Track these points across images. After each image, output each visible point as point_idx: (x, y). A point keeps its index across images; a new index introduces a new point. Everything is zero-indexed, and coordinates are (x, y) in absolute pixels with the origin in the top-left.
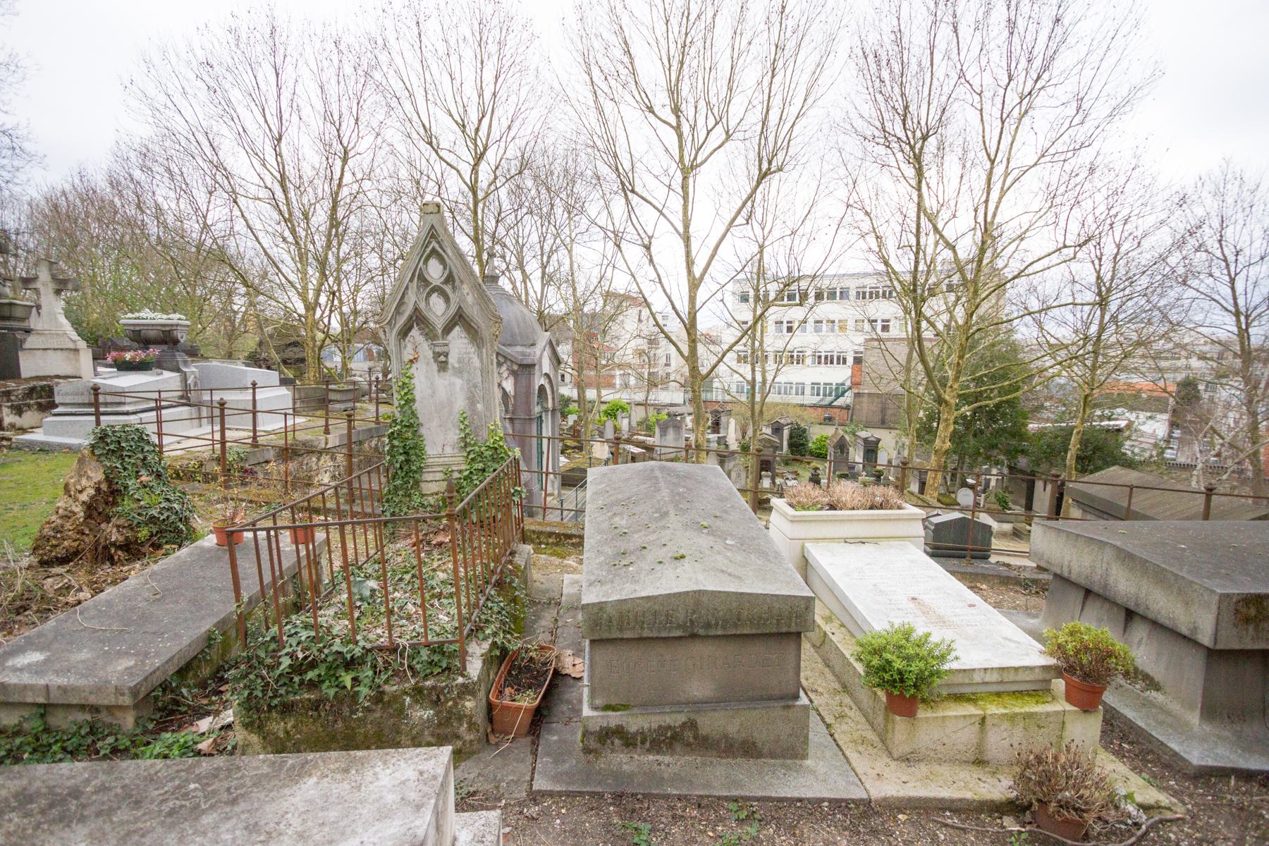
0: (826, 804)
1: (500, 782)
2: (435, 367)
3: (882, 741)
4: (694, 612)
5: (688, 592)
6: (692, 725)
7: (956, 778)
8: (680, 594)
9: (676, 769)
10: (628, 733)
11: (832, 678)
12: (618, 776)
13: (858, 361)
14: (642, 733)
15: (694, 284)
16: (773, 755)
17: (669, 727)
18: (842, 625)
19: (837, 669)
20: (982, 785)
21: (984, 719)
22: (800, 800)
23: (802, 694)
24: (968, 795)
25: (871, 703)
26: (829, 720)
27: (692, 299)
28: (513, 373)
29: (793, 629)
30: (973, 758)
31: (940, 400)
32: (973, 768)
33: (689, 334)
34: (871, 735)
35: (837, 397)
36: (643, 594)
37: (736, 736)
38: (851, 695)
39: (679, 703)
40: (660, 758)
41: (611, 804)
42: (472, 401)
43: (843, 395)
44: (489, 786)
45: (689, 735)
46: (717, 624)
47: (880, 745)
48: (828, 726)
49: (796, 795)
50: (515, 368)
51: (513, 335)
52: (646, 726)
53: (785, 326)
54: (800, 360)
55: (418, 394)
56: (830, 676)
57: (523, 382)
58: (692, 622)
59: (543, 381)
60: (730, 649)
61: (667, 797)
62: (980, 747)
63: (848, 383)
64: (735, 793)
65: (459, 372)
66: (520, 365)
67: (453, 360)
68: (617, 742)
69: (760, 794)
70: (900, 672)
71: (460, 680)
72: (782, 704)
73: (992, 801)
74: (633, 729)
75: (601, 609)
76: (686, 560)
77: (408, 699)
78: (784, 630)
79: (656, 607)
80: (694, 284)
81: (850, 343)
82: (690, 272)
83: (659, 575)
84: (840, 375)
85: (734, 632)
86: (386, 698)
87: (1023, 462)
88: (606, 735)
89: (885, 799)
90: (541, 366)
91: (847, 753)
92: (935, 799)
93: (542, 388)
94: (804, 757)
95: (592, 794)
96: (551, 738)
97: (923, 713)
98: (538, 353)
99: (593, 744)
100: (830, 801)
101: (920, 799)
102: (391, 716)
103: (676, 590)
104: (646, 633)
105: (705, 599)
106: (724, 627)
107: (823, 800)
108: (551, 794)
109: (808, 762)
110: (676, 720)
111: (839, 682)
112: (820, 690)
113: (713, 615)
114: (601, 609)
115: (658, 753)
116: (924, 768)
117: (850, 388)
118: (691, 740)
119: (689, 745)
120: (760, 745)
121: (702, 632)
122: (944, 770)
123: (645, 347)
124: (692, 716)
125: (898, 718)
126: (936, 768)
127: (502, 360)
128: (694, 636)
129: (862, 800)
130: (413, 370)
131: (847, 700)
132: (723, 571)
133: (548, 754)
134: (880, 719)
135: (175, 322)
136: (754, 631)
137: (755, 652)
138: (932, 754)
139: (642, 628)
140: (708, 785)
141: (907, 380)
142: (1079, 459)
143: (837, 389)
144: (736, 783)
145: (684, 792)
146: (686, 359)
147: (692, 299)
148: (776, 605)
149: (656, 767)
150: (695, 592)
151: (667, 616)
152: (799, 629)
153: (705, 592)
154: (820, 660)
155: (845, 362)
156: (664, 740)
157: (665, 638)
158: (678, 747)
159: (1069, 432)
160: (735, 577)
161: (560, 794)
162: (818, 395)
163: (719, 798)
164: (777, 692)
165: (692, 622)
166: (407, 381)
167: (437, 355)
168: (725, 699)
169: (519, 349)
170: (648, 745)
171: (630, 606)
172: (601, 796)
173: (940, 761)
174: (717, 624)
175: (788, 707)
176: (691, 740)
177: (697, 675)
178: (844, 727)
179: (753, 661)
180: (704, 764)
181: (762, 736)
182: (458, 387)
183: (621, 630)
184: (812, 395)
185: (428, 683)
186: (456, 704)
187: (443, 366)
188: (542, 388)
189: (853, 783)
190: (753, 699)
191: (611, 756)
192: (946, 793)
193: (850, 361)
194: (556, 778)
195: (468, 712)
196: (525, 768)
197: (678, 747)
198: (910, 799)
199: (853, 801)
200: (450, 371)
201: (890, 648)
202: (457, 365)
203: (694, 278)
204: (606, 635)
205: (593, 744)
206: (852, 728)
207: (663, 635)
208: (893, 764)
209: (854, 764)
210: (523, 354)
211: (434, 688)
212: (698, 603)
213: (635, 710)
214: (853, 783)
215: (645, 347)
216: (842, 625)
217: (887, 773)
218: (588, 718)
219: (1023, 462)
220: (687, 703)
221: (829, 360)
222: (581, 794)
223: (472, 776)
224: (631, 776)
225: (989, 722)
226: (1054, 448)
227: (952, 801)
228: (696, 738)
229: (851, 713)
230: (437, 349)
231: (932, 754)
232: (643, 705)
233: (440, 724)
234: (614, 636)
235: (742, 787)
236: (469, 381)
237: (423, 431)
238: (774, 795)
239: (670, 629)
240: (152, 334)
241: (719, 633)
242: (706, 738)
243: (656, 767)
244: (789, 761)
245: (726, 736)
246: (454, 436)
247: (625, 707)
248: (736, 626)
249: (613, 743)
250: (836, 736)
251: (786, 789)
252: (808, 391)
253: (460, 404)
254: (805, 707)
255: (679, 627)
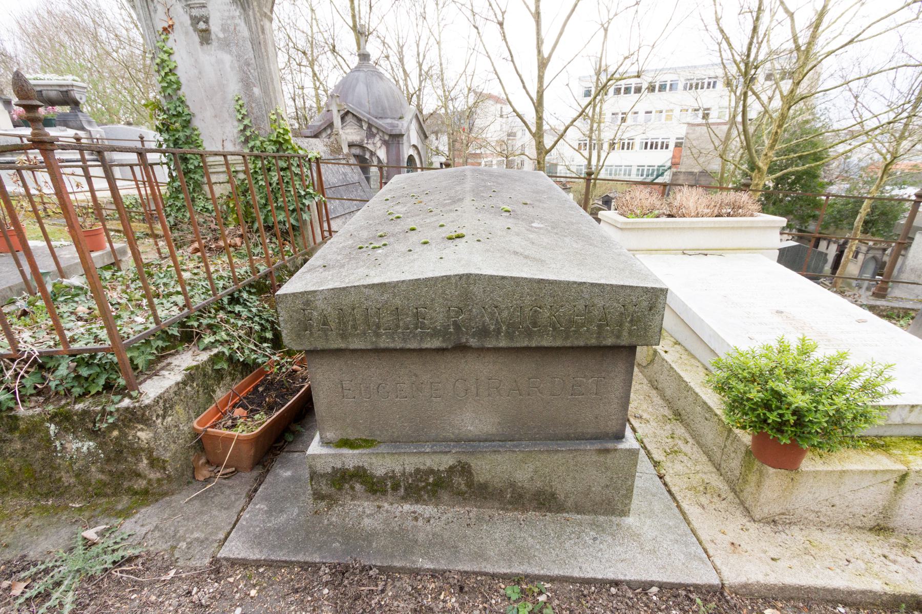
0: (655, 589)
1: (179, 541)
2: (196, 38)
3: (733, 490)
4: (460, 310)
5: (448, 277)
6: (464, 470)
7: (849, 555)
8: (435, 280)
9: (436, 526)
10: (372, 476)
11: (661, 402)
12: (354, 537)
13: (678, 145)
14: (393, 477)
15: (543, 64)
16: (579, 510)
17: (431, 471)
18: (677, 343)
19: (668, 393)
20: (893, 567)
21: (904, 477)
22: (616, 583)
23: (628, 432)
24: (877, 586)
25: (720, 441)
26: (658, 455)
27: (541, 78)
28: (385, 143)
29: (625, 341)
30: (873, 523)
31: (753, 167)
32: (872, 537)
33: (537, 111)
34: (716, 481)
35: (658, 176)
36: (376, 281)
37: (526, 485)
38: (687, 426)
39: (445, 440)
40: (419, 508)
41: (326, 584)
42: (247, 84)
43: (662, 174)
44: (162, 546)
45: (459, 481)
46: (498, 331)
47: (731, 496)
48: (656, 464)
49: (611, 575)
50: (387, 138)
51: (383, 109)
52: (398, 469)
53: (620, 116)
54: (629, 146)
55: (183, 74)
56: (657, 400)
57: (393, 151)
58: (457, 326)
59: (412, 152)
60: (525, 367)
61: (415, 573)
62: (887, 512)
63: (669, 164)
64: (518, 569)
65: (225, 44)
66: (390, 135)
67: (215, 27)
68: (358, 486)
69: (556, 571)
70: (797, 412)
71: (126, 402)
72: (598, 446)
73: (913, 596)
74: (380, 472)
75: (307, 303)
76: (463, 240)
77: (53, 427)
78: (609, 342)
79: (398, 302)
80: (543, 64)
81: (674, 131)
82: (539, 52)
83: (416, 256)
84: (662, 158)
85: (525, 343)
86: (22, 426)
87: (812, 226)
88: (342, 479)
89: (745, 586)
90: (409, 136)
91: (685, 505)
92: (825, 590)
93: (411, 158)
94: (624, 513)
95: (304, 566)
96: (283, 473)
97: (809, 464)
98: (405, 125)
99: (325, 489)
100: (661, 586)
101: (799, 589)
102: (37, 448)
103: (430, 275)
104: (384, 342)
105: (477, 290)
106: (510, 336)
107: (651, 584)
108: (244, 563)
109: (630, 520)
110: (444, 462)
111: (671, 408)
112: (645, 416)
113: (492, 314)
114: (307, 303)
115: (417, 502)
116: (797, 535)
117: (670, 168)
118: (463, 487)
119: (460, 494)
120: (562, 497)
121: (473, 342)
122: (827, 538)
123: (505, 139)
124: (464, 459)
125: (771, 470)
126: (816, 535)
127: (374, 130)
128: (462, 349)
129: (711, 586)
130: (170, 44)
131: (680, 430)
132: (516, 253)
133: (266, 499)
134: (735, 464)
135: (69, 82)
136: (559, 343)
137: (563, 371)
138: (812, 516)
139: (378, 335)
140: (480, 555)
141: (725, 150)
142: (866, 223)
143: (658, 170)
144: (523, 553)
145: (442, 565)
146: (534, 135)
147: (541, 78)
148: (600, 303)
149: (409, 523)
150: (461, 277)
151: (417, 315)
152: (634, 341)
153: (479, 277)
154: (645, 381)
155: (667, 147)
156: (423, 487)
157: (414, 350)
158: (445, 496)
159: (859, 201)
160: (535, 259)
161: (258, 564)
162: (642, 175)
163: (493, 576)
164: (591, 430)
165: (457, 326)
166: (165, 57)
167: (195, 20)
168: (506, 439)
169: (389, 121)
170: (402, 491)
171: (352, 298)
172: (316, 567)
173: (822, 526)
174: (498, 331)
175: (607, 451)
176: (463, 487)
177: (471, 404)
178: (679, 467)
179: (553, 389)
180: (480, 519)
181: (564, 487)
182: (228, 65)
183: (344, 336)
184: (638, 175)
185: (79, 407)
186: (124, 435)
187: (205, 36)
188: (411, 158)
189: (696, 557)
190: (555, 438)
191: (350, 504)
192: (840, 581)
193: (672, 146)
194: (257, 540)
195: (144, 445)
196: (223, 518)
197: (445, 496)
198: (783, 589)
199: (697, 588)
200: (215, 44)
201: (779, 372)
202: (221, 35)
203: (543, 58)
204: (320, 345)
205: (325, 489)
206: (687, 469)
207: (413, 345)
208: (752, 526)
209: (696, 524)
210: (393, 125)
211: (85, 413)
212: (466, 296)
213: (382, 449)
214: (696, 557)
215: (505, 139)
216: (677, 343)
217: (744, 539)
218: (314, 457)
219: (812, 226)
220: (458, 441)
221: (654, 146)
222: (288, 564)
223: (144, 530)
224: (369, 537)
225: (909, 481)
226: (844, 214)
227: (850, 593)
228: (470, 484)
229: (686, 448)
230: (195, 12)
231: (812, 516)
232: (394, 441)
233: (108, 460)
234: (334, 346)
235: (530, 559)
236: (239, 57)
237: (196, 123)
238: (576, 574)
239: (423, 336)
240: (53, 94)
241: (503, 344)
242: (484, 487)
243: (409, 523)
244: (601, 518)
245: (512, 485)
246: (232, 129)
247: (367, 443)
248: (529, 334)
249: (352, 488)
250: (667, 479)
251: (596, 564)
252: (634, 171)
253: (234, 88)
254: (633, 453)
255: (435, 333)
